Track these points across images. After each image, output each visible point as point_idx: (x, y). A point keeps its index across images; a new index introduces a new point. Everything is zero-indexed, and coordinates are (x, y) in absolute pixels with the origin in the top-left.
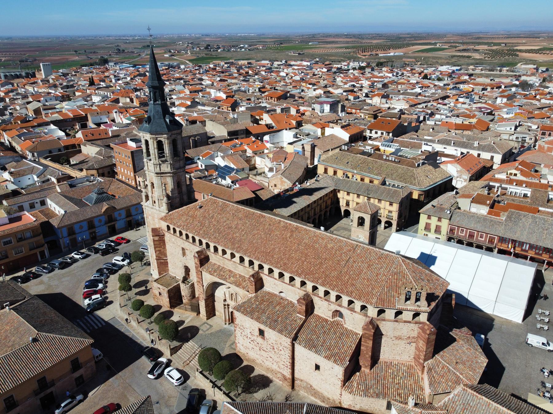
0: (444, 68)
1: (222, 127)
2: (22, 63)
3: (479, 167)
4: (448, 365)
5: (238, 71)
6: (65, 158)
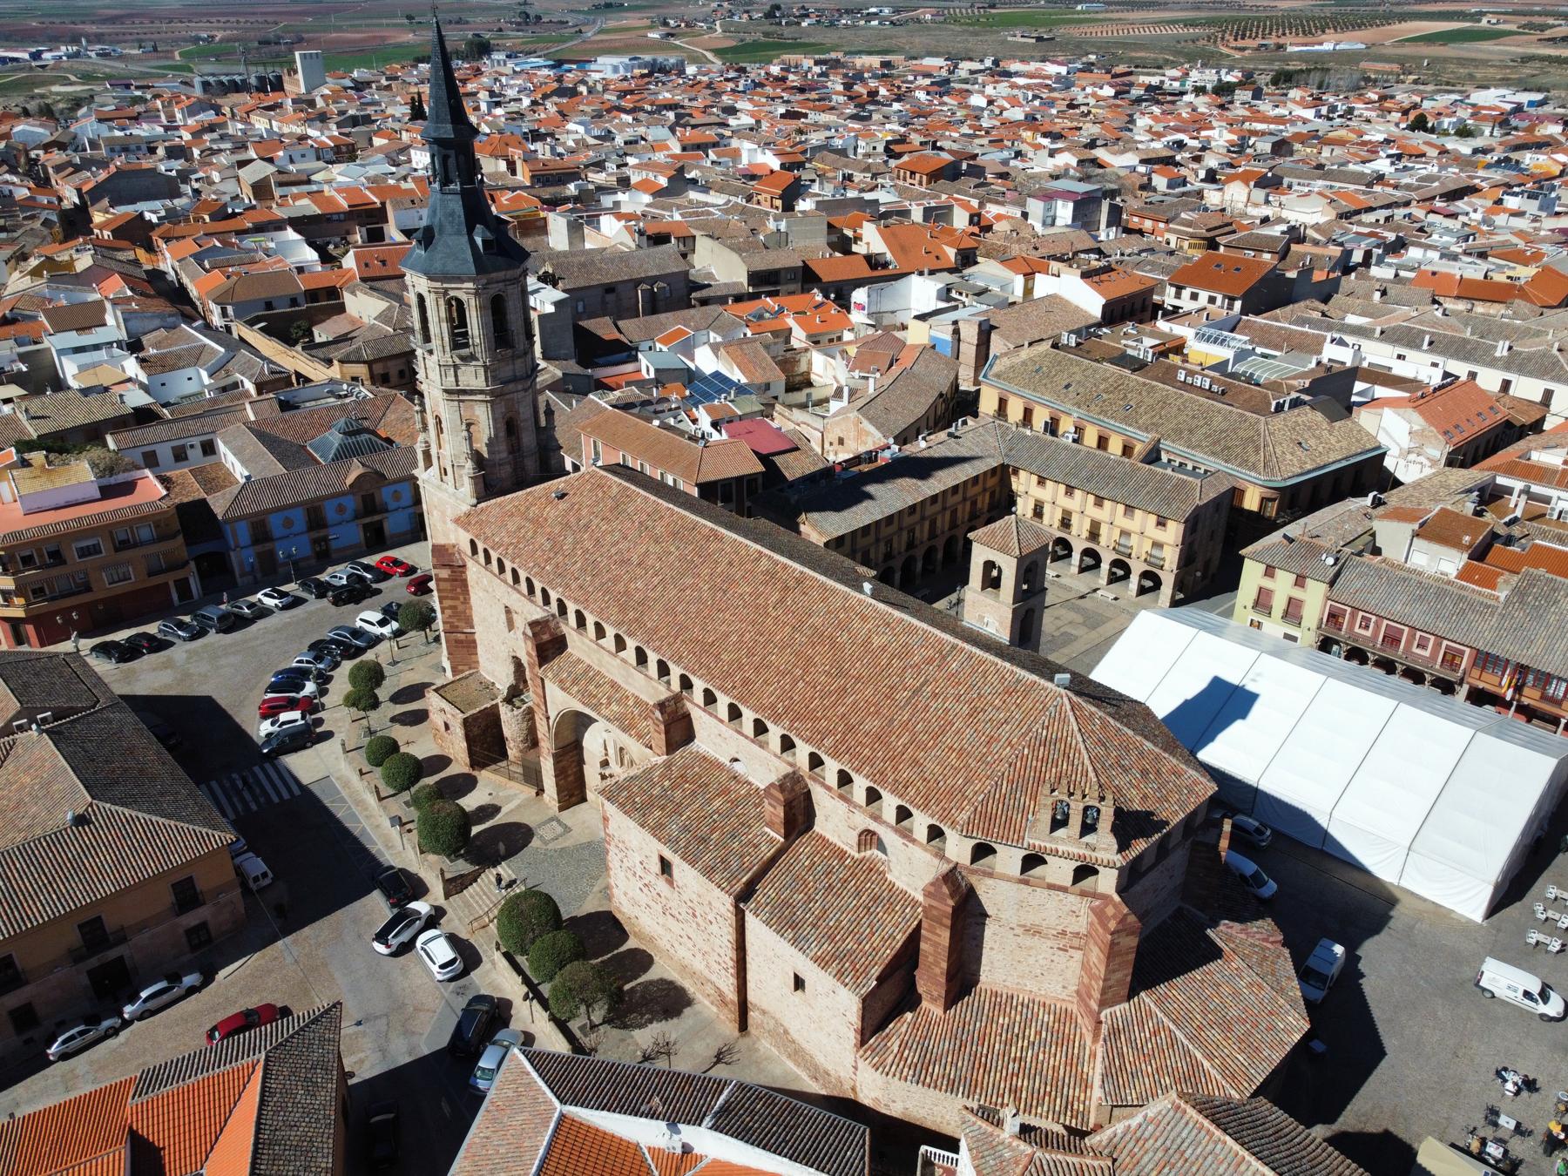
0: (1492, 98)
1: (735, 257)
2: (265, 49)
3: (1487, 422)
4: (1172, 1027)
5: (848, 87)
6: (304, 324)
